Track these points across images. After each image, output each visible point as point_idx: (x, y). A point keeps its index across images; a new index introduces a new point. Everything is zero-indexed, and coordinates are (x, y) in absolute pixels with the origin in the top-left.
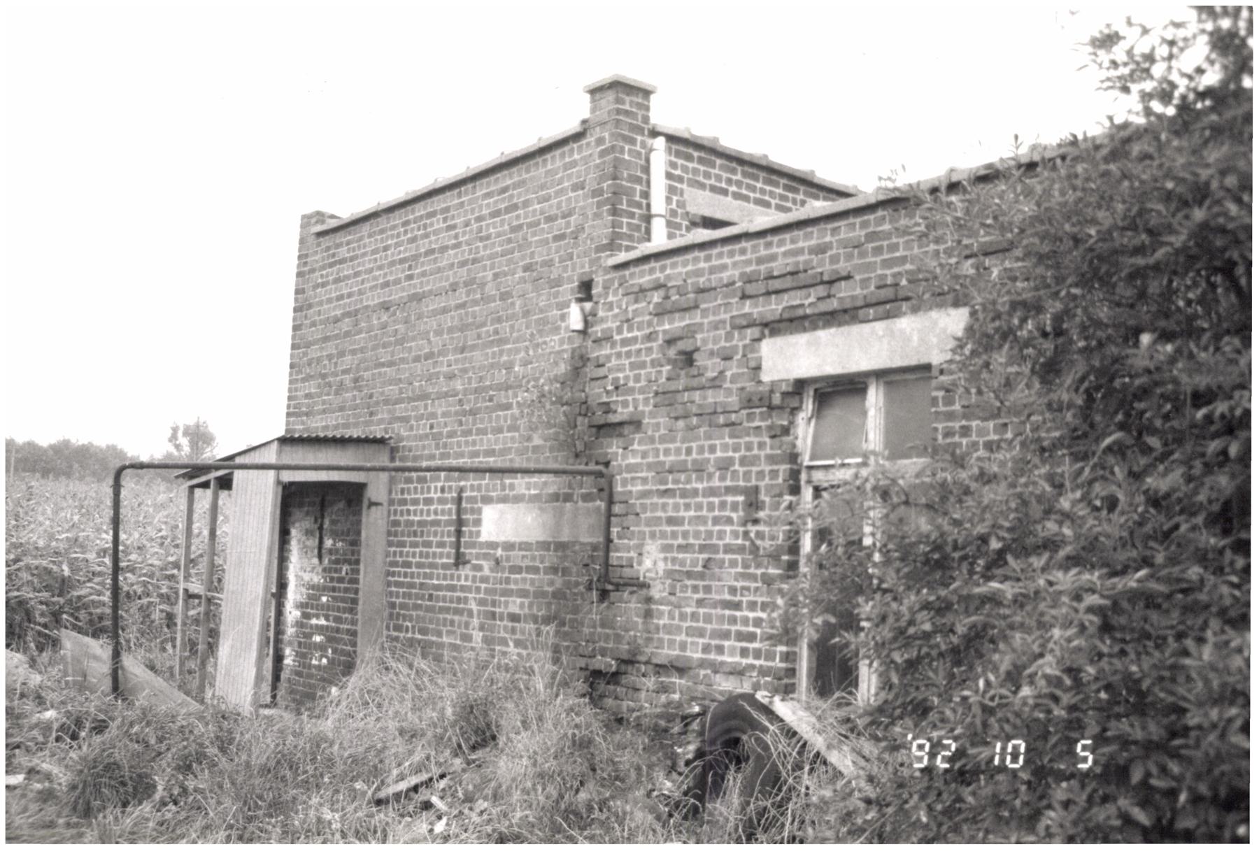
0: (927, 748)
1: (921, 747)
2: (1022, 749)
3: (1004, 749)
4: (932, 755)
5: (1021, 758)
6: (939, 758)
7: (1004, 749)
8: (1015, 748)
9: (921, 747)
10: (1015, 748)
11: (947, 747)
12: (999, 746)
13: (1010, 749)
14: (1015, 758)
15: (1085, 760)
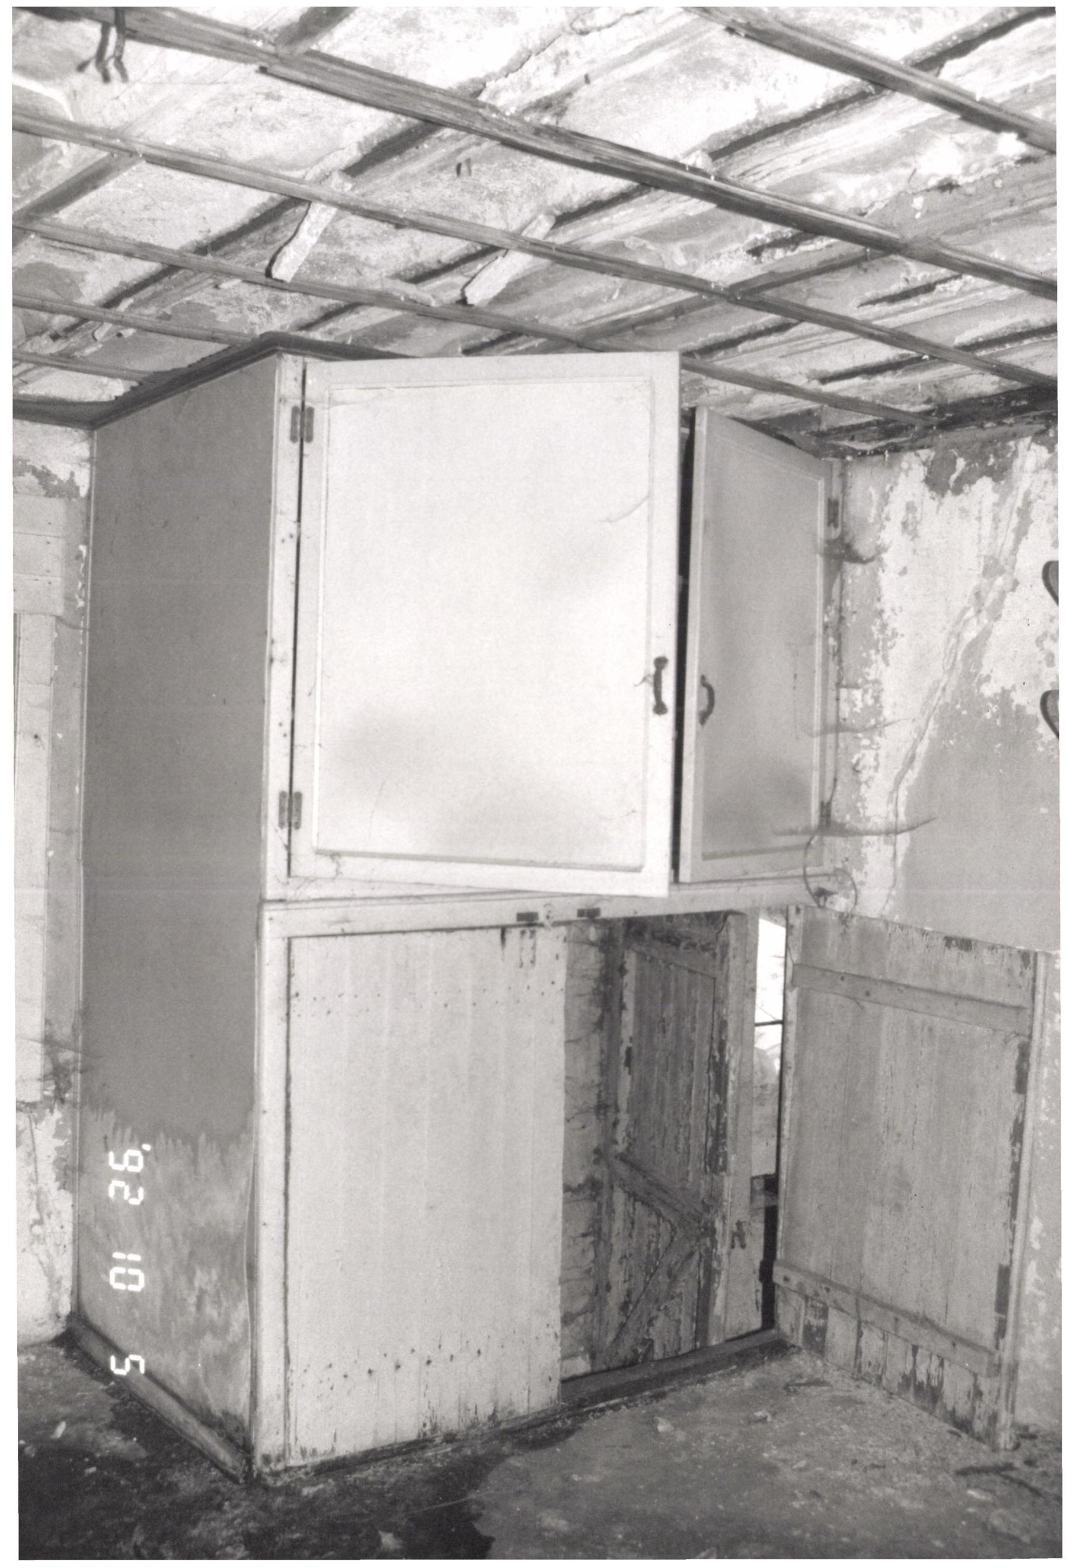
1: (133, 1161)
2: (132, 1288)
4: (125, 1176)
5: (120, 1286)
6: (121, 1184)
8: (135, 1280)
9: (133, 1161)
10: (135, 1280)
11: (134, 1194)
12: (136, 1258)
13: (133, 1272)
14: (119, 1278)
15: (120, 1365)
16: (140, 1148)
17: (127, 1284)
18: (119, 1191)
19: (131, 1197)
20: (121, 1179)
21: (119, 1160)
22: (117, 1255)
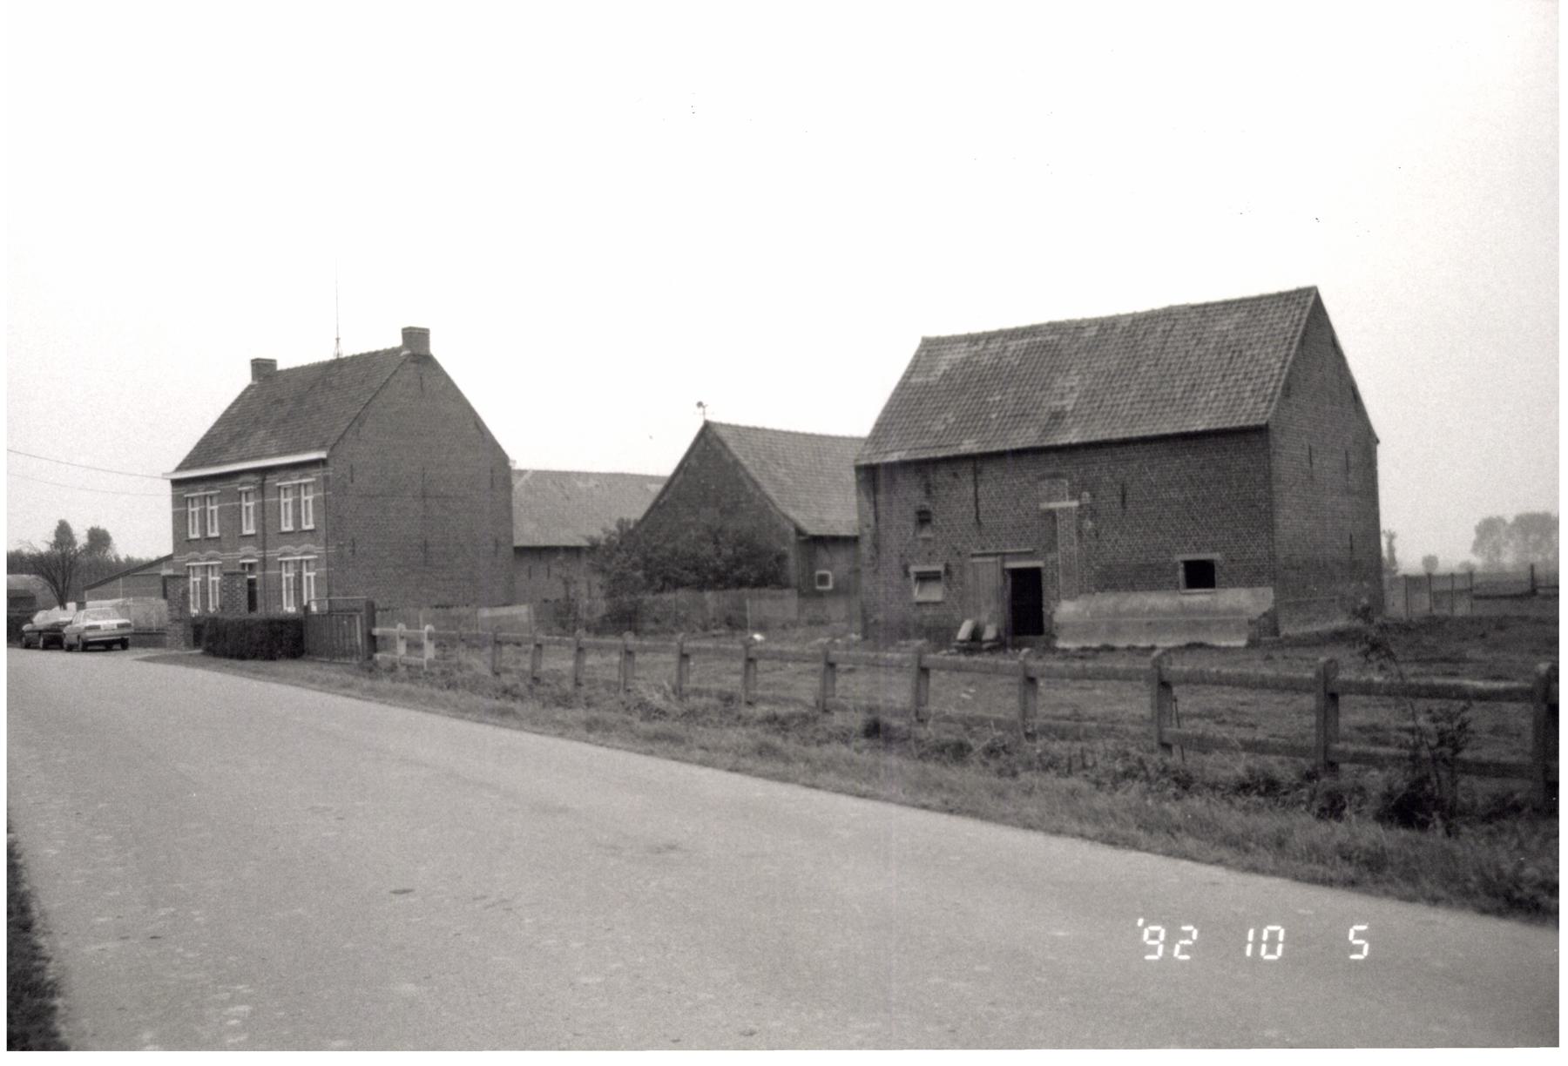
0: (1162, 936)
1: (1154, 936)
2: (1281, 938)
3: (1258, 935)
4: (1169, 943)
5: (1280, 948)
6: (1177, 948)
7: (1258, 935)
8: (1274, 935)
9: (1154, 936)
10: (1274, 935)
11: (1188, 935)
12: (1251, 935)
13: (1265, 937)
14: (1271, 951)
17: (1267, 942)
18: (1185, 950)
19: (1191, 939)
21: (1153, 950)
22: (1249, 951)
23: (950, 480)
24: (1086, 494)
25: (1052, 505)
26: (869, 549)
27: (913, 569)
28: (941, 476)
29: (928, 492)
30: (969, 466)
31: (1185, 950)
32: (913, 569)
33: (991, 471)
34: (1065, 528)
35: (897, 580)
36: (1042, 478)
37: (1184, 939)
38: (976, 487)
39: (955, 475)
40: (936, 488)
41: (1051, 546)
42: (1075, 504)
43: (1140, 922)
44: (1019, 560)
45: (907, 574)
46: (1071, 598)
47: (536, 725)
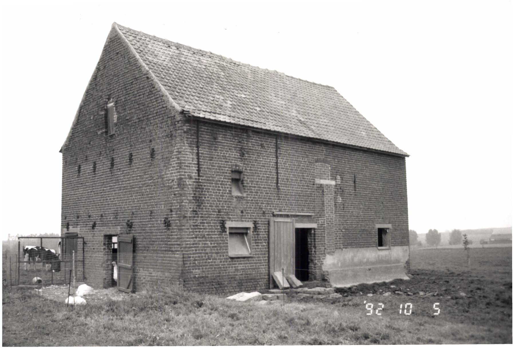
0: (372, 307)
1: (370, 307)
4: (375, 309)
6: (377, 311)
8: (409, 306)
9: (370, 307)
11: (381, 306)
13: (406, 307)
14: (408, 312)
15: (437, 306)
16: (365, 305)
17: (407, 309)
20: (375, 312)
21: (369, 312)
23: (259, 148)
24: (338, 177)
25: (323, 182)
26: (190, 202)
27: (229, 224)
28: (253, 143)
29: (242, 155)
30: (271, 142)
31: (379, 312)
32: (229, 224)
33: (285, 147)
34: (328, 198)
35: (216, 236)
36: (317, 161)
37: (379, 308)
38: (277, 158)
39: (262, 146)
40: (248, 153)
41: (321, 214)
42: (333, 183)
43: (365, 302)
44: (302, 222)
45: (223, 227)
46: (331, 253)
47: (77, 114)
